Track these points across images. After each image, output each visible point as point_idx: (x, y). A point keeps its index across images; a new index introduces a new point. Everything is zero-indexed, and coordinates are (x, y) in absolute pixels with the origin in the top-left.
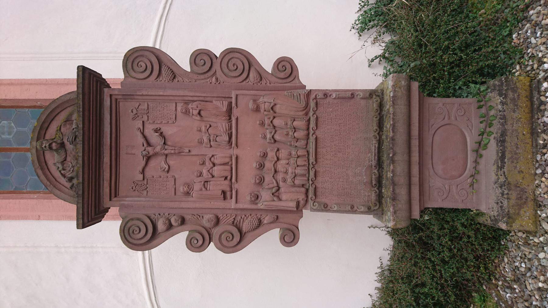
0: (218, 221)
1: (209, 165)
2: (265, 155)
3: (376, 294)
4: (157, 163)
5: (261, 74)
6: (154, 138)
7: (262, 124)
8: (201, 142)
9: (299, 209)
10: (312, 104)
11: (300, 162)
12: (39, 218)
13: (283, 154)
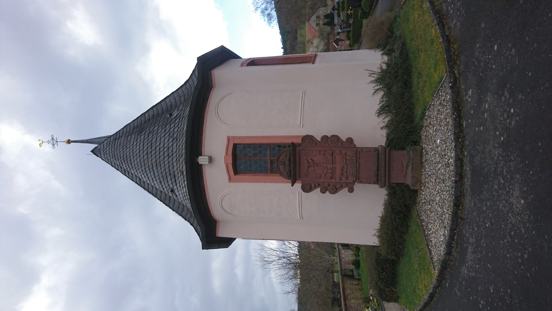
2: (344, 167)
3: (383, 211)
5: (342, 142)
6: (310, 161)
7: (343, 158)
9: (354, 182)
10: (358, 153)
11: (355, 169)
12: (265, 182)
13: (349, 167)
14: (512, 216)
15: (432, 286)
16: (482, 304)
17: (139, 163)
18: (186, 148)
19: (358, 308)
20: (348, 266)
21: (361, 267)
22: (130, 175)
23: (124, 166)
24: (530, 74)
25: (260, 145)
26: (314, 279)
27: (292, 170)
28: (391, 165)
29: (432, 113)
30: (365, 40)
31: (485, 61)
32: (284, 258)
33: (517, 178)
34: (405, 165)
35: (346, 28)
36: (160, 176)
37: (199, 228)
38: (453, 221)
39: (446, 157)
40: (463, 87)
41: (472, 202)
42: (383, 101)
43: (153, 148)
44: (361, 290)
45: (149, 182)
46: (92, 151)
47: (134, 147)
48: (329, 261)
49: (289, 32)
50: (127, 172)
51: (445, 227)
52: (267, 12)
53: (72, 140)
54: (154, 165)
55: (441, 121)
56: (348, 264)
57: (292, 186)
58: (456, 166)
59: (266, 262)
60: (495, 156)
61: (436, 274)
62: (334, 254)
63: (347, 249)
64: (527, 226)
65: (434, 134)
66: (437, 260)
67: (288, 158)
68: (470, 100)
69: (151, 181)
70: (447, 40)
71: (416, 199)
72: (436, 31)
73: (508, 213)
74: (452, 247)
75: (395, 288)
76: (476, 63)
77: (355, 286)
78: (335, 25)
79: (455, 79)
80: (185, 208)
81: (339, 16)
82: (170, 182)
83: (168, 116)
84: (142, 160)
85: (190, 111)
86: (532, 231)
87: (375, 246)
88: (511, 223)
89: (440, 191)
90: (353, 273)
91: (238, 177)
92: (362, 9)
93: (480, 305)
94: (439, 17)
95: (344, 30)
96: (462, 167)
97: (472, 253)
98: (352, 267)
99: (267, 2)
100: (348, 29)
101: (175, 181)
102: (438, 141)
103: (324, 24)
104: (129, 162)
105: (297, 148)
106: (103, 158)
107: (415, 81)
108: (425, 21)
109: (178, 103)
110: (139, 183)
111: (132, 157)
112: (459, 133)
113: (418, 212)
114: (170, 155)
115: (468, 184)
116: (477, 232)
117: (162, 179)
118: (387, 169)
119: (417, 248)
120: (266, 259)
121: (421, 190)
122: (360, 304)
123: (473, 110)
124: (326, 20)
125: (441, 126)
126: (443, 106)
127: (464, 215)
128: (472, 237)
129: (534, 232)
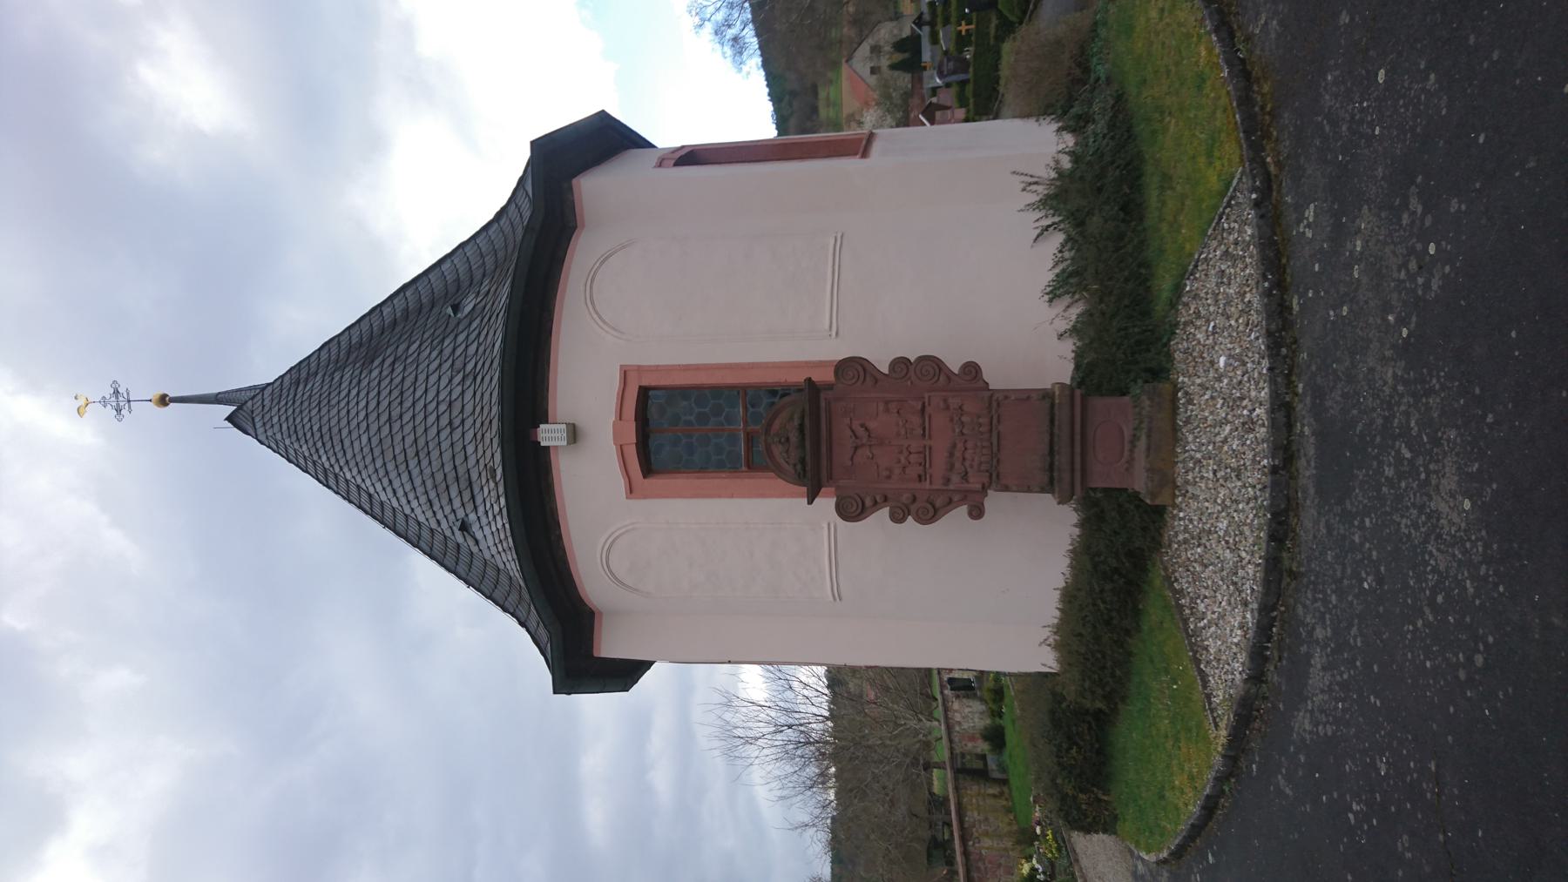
0: (914, 499)
1: (905, 453)
2: (954, 446)
3: (1067, 571)
4: (864, 453)
5: (950, 375)
6: (861, 432)
8: (898, 434)
9: (984, 491)
10: (994, 404)
13: (970, 444)
14: (1438, 550)
15: (1210, 775)
16: (1356, 814)
17: (366, 450)
18: (501, 402)
19: (1002, 861)
20: (970, 745)
21: (1009, 744)
22: (342, 484)
23: (324, 458)
24: (1481, 140)
25: (717, 391)
26: (876, 786)
27: (808, 459)
28: (1089, 441)
29: (1203, 285)
30: (1009, 92)
31: (1353, 116)
32: (790, 727)
33: (1448, 440)
34: (1127, 434)
35: (954, 72)
36: (429, 484)
37: (543, 633)
38: (1267, 582)
39: (1245, 402)
40: (1289, 199)
41: (1322, 525)
42: (1063, 260)
43: (407, 404)
44: (1009, 810)
45: (395, 504)
46: (230, 419)
47: (352, 404)
48: (917, 733)
49: (793, 94)
50: (331, 476)
51: (1245, 604)
52: (731, 33)
53: (172, 395)
54: (411, 452)
55: (1228, 303)
56: (972, 738)
57: (810, 502)
58: (1274, 425)
59: (735, 741)
60: (1385, 383)
61: (1223, 740)
62: (931, 714)
63: (967, 697)
64: (1482, 572)
65: (1210, 341)
66: (1225, 700)
67: (796, 422)
68: (1309, 234)
69: (403, 501)
70: (1244, 73)
71: (1161, 535)
72: (1210, 50)
73: (1426, 541)
74: (1266, 659)
75: (1107, 792)
76: (1327, 128)
77: (990, 801)
78: (925, 68)
79: (1268, 180)
80: (503, 579)
81: (934, 40)
82: (457, 503)
83: (450, 311)
84: (375, 441)
85: (511, 296)
86: (1496, 585)
87: (1046, 675)
88: (1435, 570)
89: (1228, 503)
90: (986, 764)
91: (655, 482)
92: (1001, 15)
93: (1351, 816)
94: (1220, 11)
95: (949, 79)
96: (1290, 426)
97: (1324, 669)
98: (983, 747)
99: (731, 6)
100: (962, 77)
101: (473, 497)
102: (1222, 360)
103: (893, 67)
104: (338, 448)
105: (822, 395)
106: (262, 438)
107: (1152, 197)
108: (1180, 25)
109: (478, 275)
110: (367, 507)
111: (345, 432)
112: (1279, 331)
113: (1166, 569)
114: (457, 422)
115: (1308, 473)
116: (1335, 607)
117: (432, 495)
118: (1078, 449)
119: (1167, 672)
120: (739, 732)
121: (1175, 506)
122: (1006, 849)
123: (1319, 261)
124: (899, 57)
125: (1228, 318)
126: (1234, 259)
127: (1300, 564)
128: (1324, 623)
129: (1501, 589)
